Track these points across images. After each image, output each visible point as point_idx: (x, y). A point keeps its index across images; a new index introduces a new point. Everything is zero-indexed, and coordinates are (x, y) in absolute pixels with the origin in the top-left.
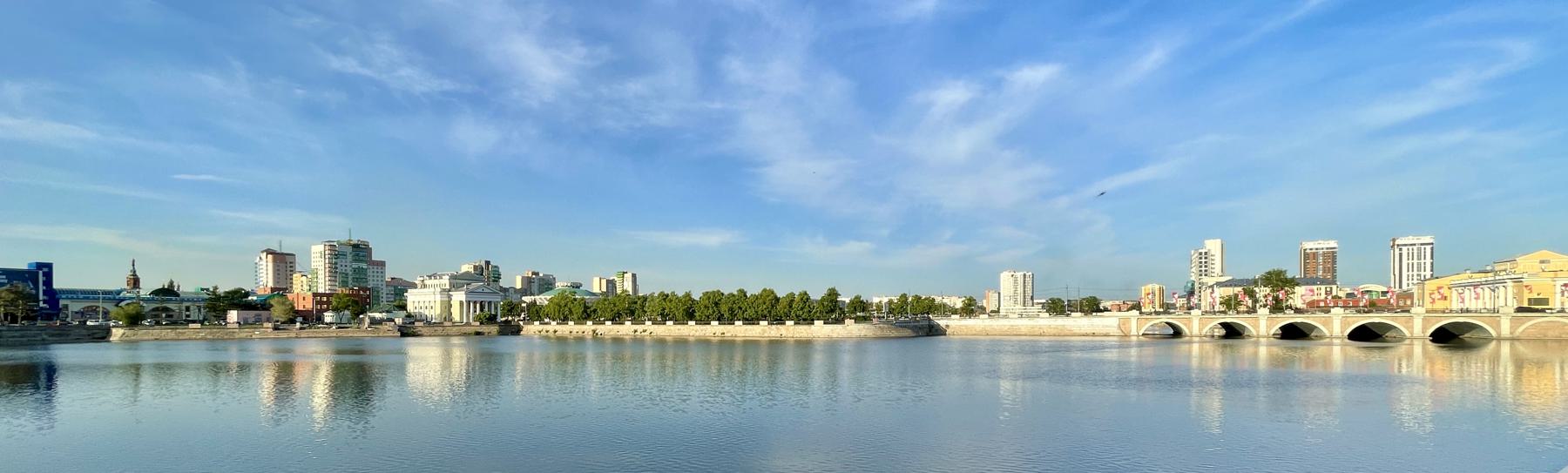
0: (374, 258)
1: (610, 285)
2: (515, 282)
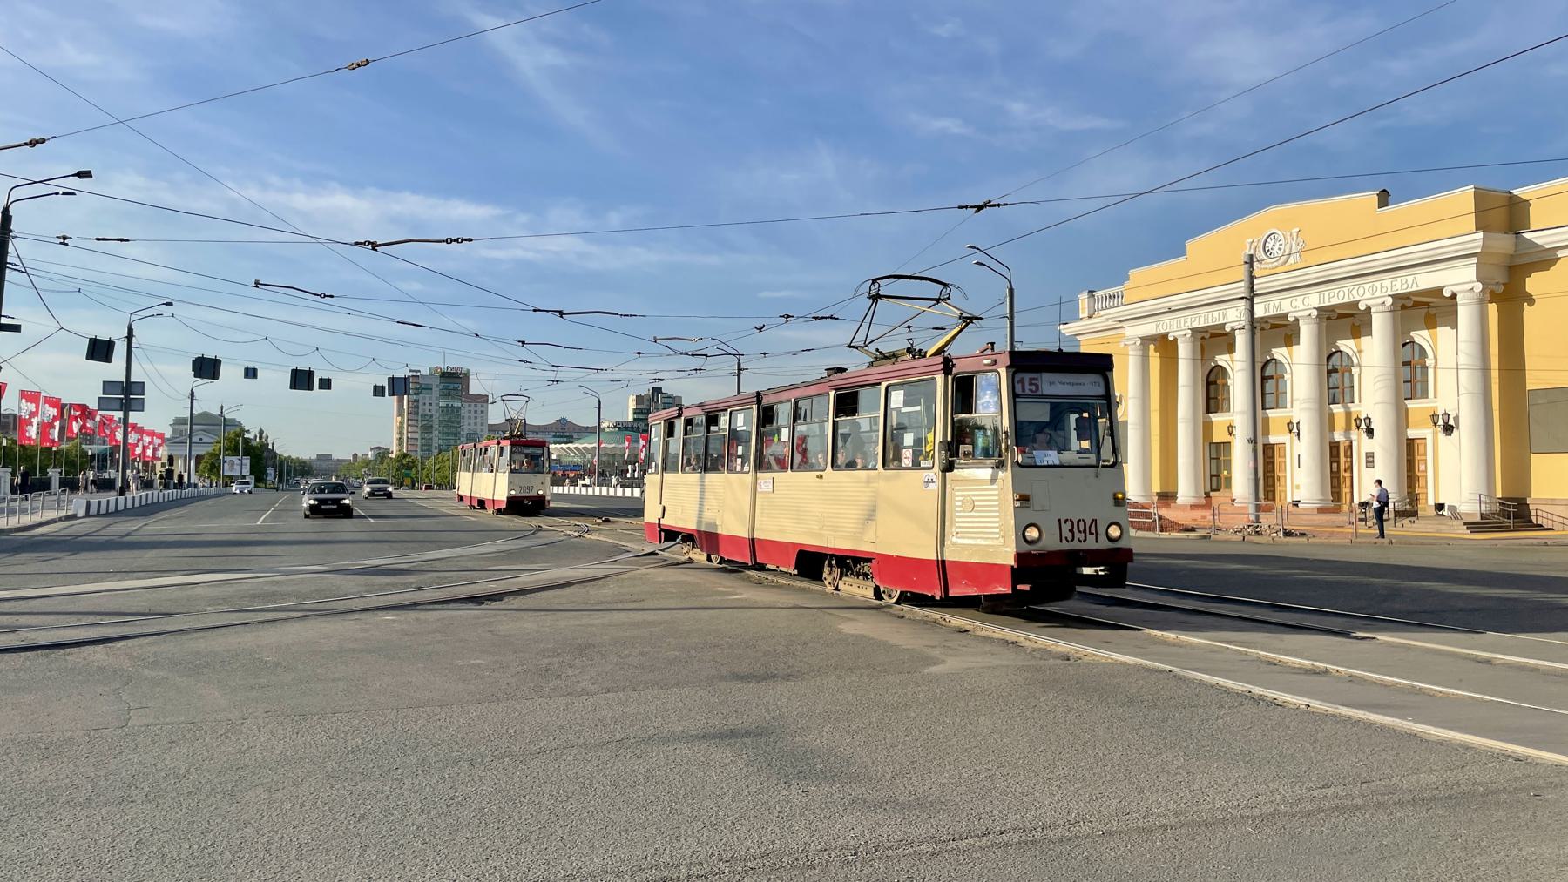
0: (472, 391)
1: (1214, 479)
2: (1417, 426)
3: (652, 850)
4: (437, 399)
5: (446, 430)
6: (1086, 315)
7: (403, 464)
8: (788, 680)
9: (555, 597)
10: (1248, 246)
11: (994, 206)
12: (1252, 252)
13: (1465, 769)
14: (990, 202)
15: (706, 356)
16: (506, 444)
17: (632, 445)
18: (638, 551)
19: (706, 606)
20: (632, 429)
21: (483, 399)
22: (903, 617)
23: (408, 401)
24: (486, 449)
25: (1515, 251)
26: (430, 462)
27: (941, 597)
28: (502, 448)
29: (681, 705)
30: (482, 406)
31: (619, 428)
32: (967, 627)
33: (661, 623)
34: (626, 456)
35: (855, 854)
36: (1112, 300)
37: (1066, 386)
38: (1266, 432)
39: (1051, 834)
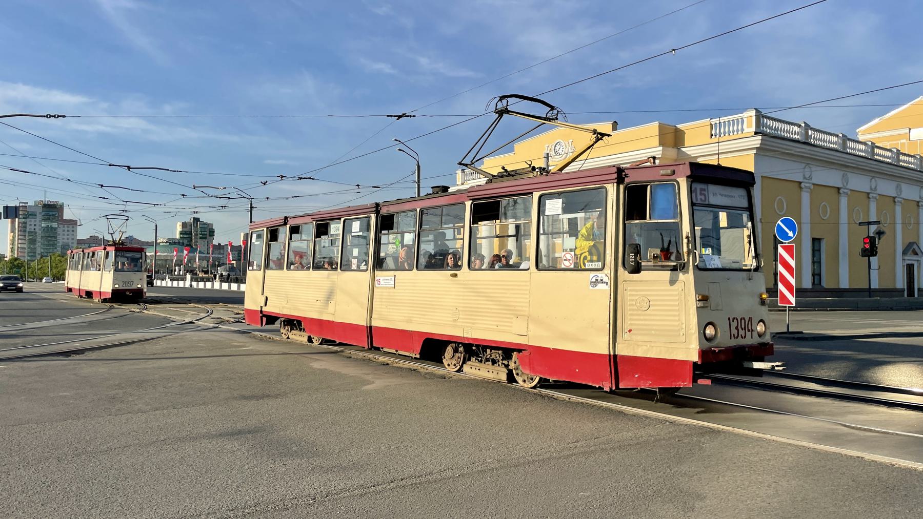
0: (65, 217)
3: (183, 507)
4: (40, 222)
5: (46, 243)
6: (460, 183)
7: (14, 265)
8: (277, 398)
9: (121, 352)
10: (546, 148)
11: (408, 116)
12: (548, 152)
13: (645, 429)
14: (405, 114)
15: (229, 198)
16: (111, 250)
17: (179, 254)
18: (181, 321)
19: (225, 354)
20: (179, 244)
21: (73, 223)
22: (350, 357)
23: (19, 223)
24: (94, 254)
25: (678, 157)
26: (34, 264)
27: (611, 389)
28: (108, 253)
29: (206, 416)
30: (73, 227)
31: (170, 243)
32: (389, 362)
33: (195, 366)
34: (174, 260)
35: (314, 499)
36: (474, 175)
37: (724, 197)
38: (554, 252)
39: (430, 478)
